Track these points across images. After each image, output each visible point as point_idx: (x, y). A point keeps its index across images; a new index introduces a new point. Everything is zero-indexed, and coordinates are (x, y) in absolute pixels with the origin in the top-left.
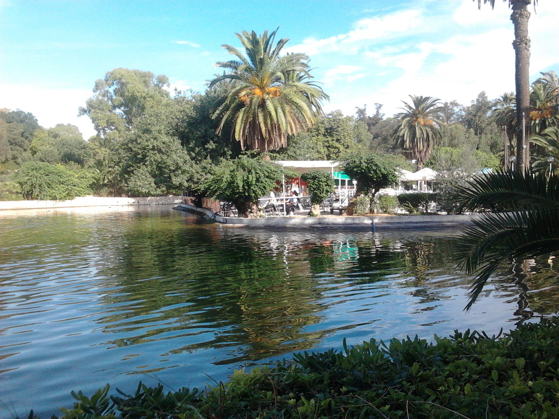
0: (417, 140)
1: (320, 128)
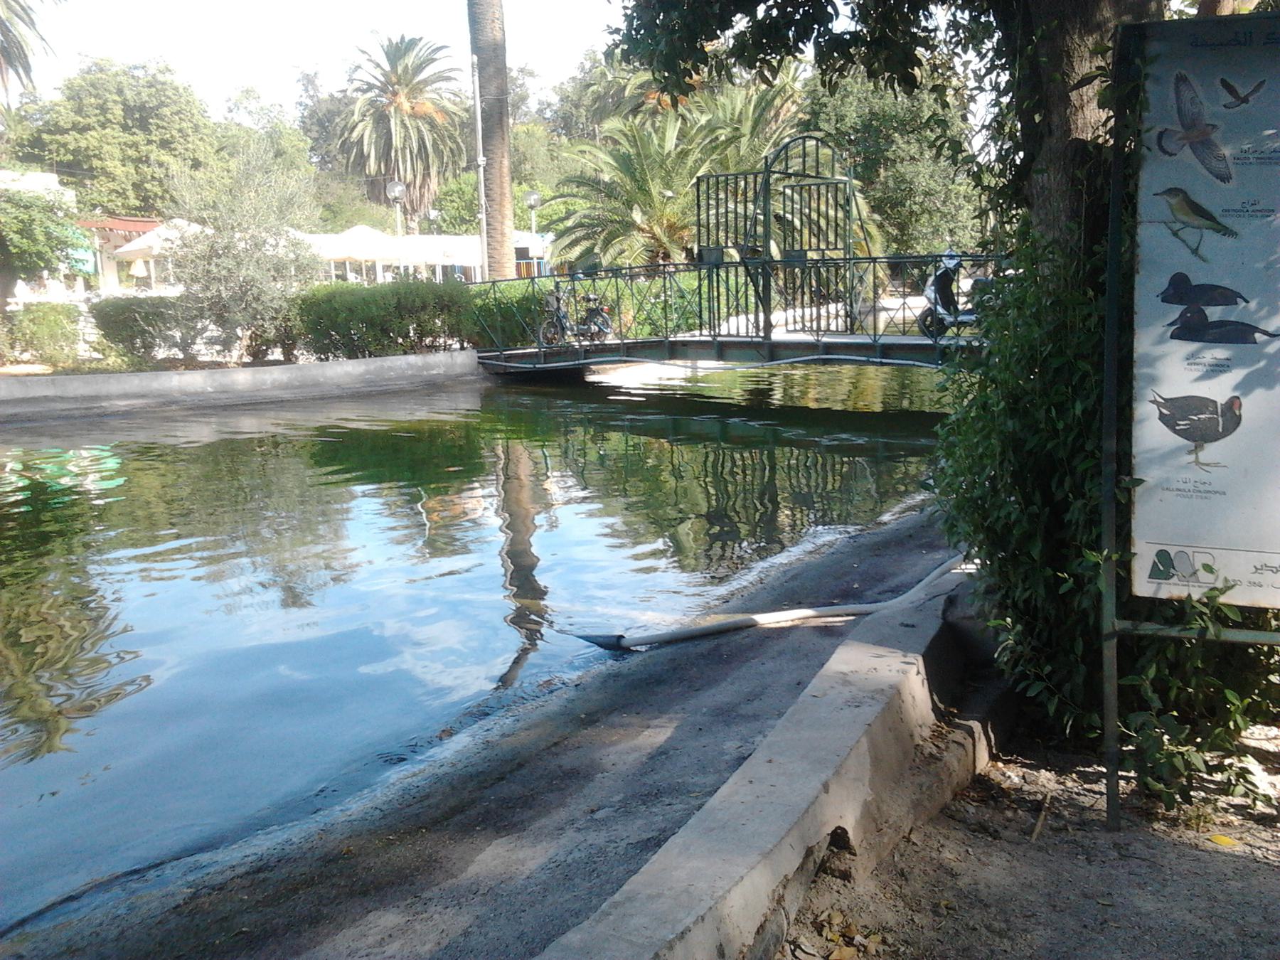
0: (396, 155)
1: (110, 105)
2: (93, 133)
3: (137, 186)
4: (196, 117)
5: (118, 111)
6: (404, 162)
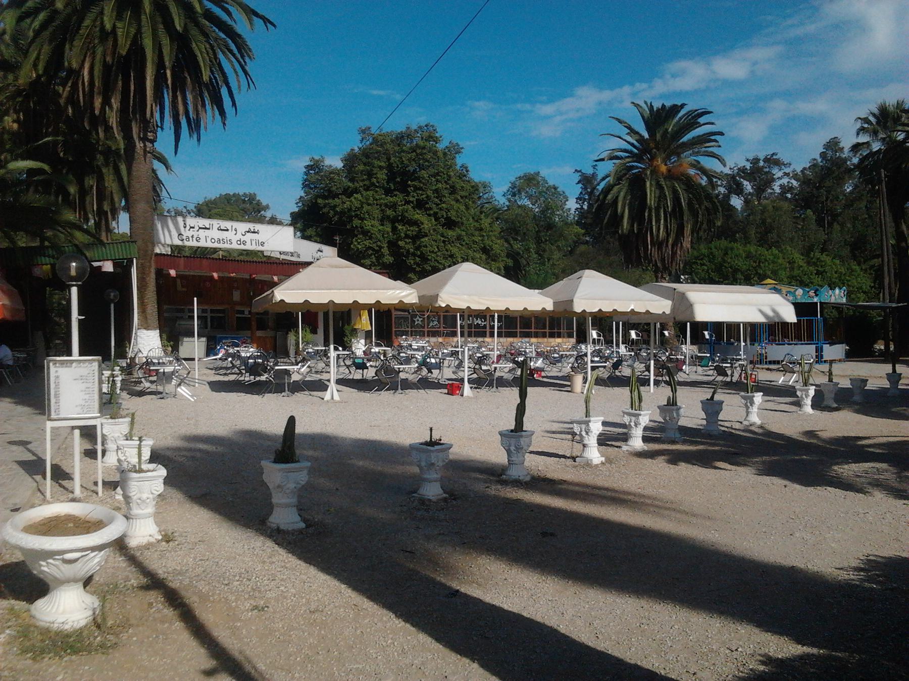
2: (358, 196)
3: (393, 245)
4: (453, 179)
5: (382, 175)
6: (658, 221)
